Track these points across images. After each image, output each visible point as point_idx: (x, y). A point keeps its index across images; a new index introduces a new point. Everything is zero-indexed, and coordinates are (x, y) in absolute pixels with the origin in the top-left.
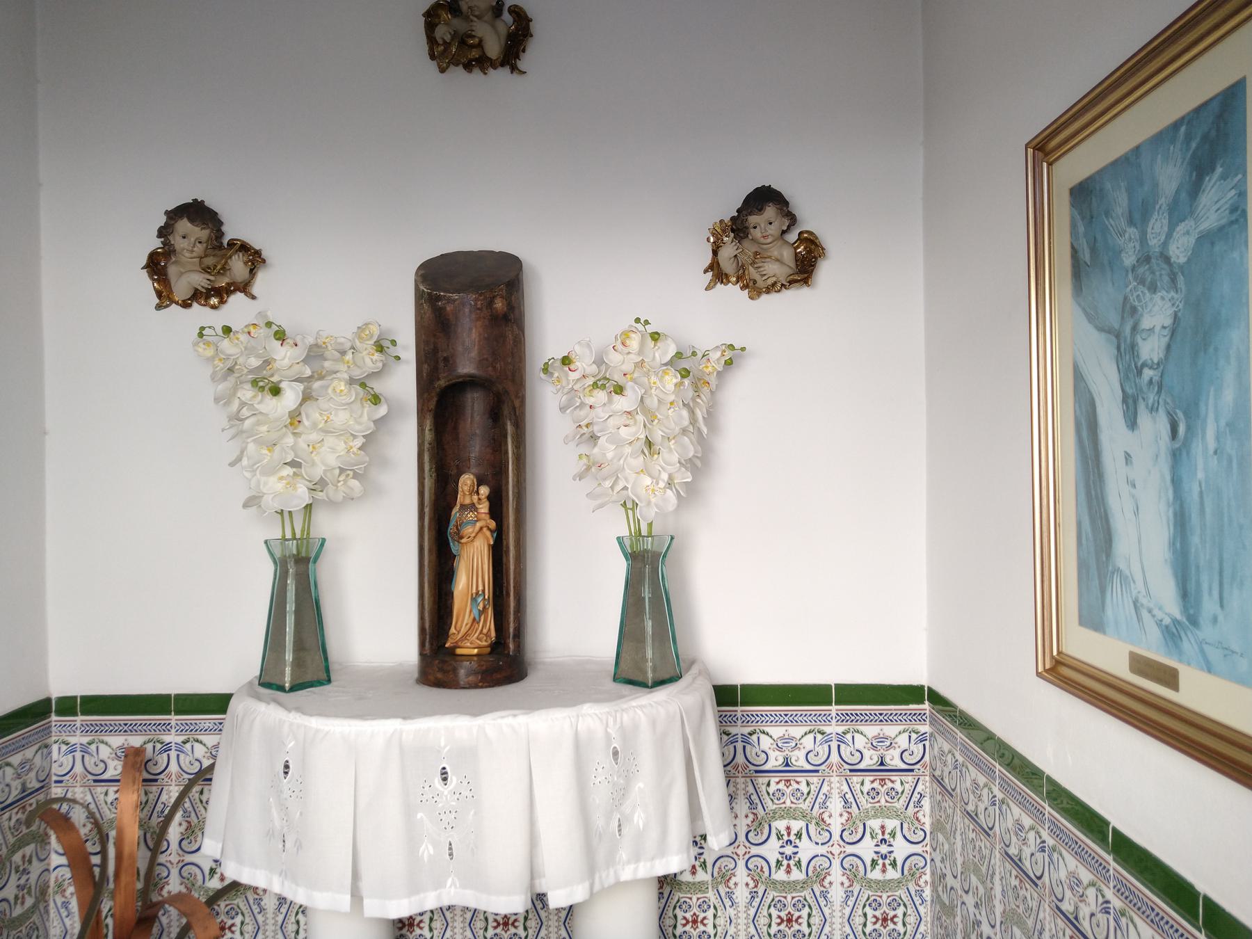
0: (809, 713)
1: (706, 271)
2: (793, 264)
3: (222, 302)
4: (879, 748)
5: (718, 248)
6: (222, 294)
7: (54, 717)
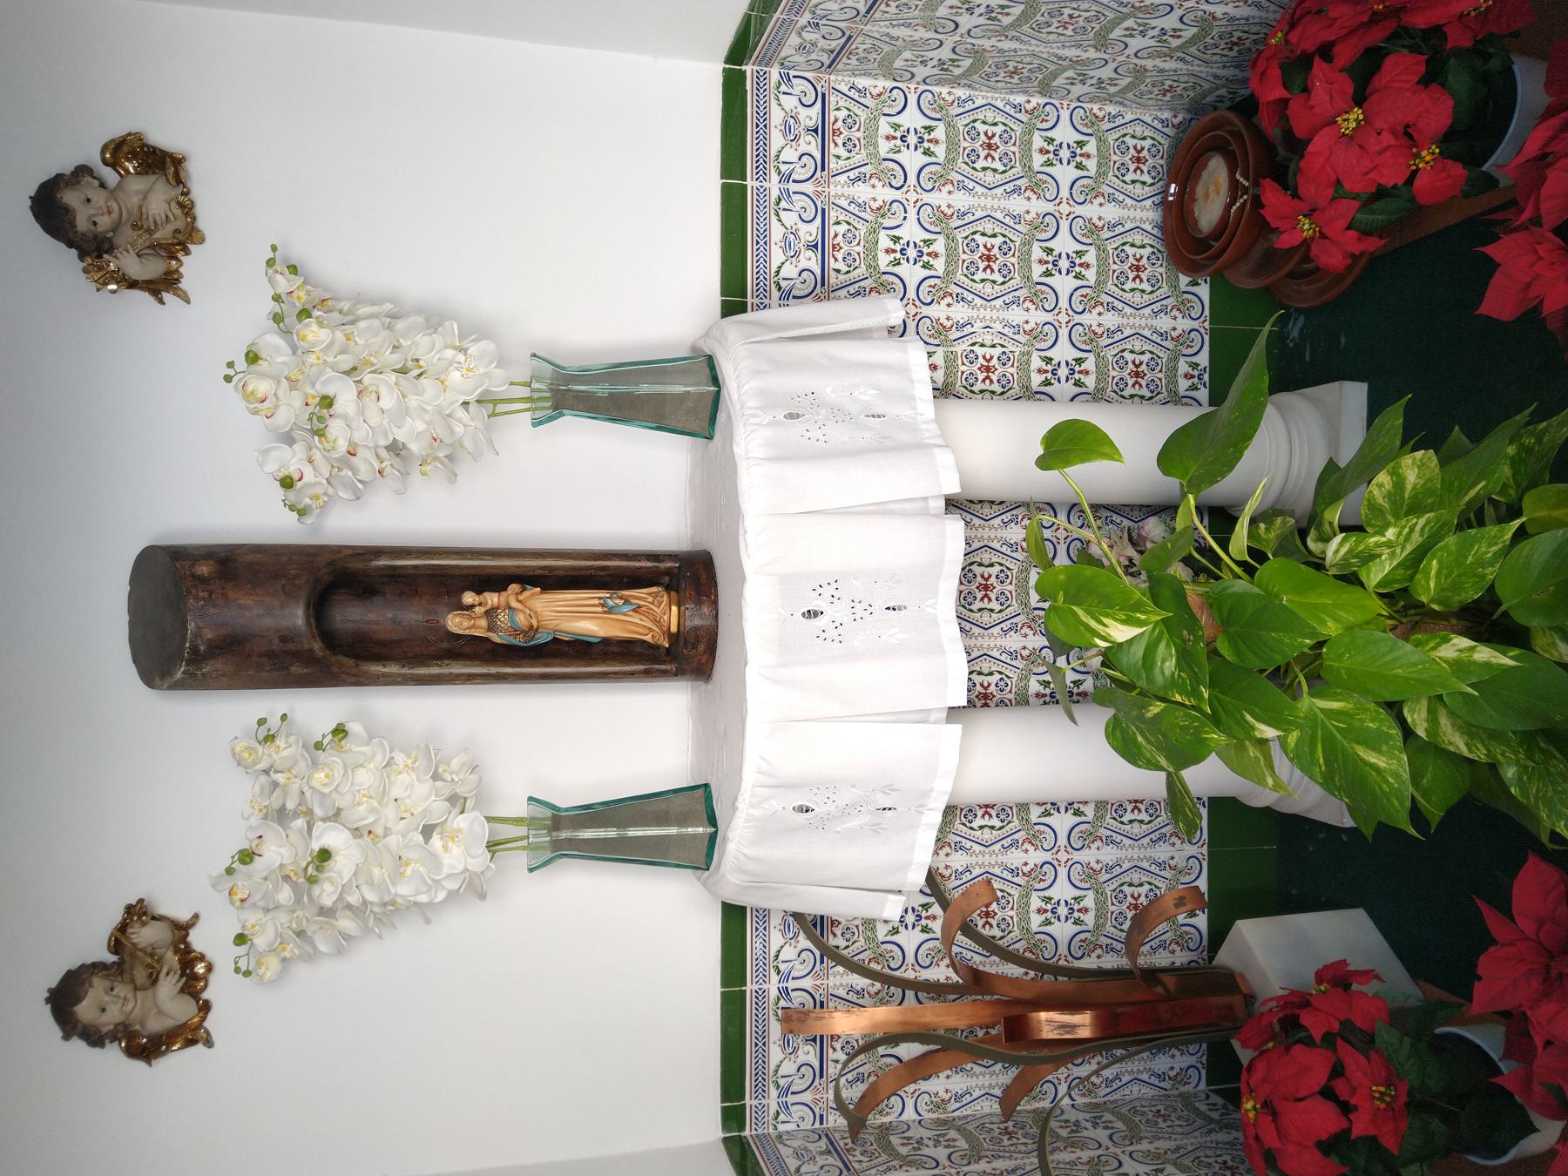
0: (755, 214)
1: (161, 302)
2: (152, 178)
3: (202, 958)
4: (796, 132)
5: (126, 280)
6: (188, 959)
7: (747, 1133)
